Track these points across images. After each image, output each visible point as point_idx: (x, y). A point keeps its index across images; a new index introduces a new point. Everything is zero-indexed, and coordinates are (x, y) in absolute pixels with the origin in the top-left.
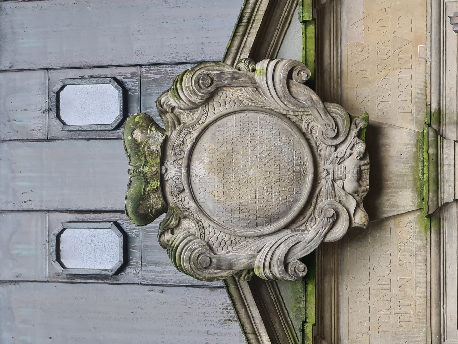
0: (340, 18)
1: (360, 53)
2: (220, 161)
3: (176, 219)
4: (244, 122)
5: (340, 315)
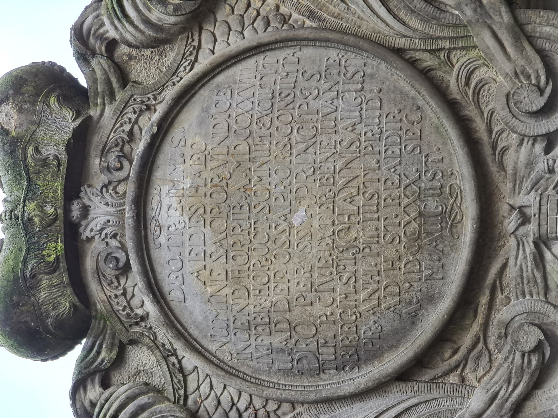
3: (110, 346)
4: (285, 74)
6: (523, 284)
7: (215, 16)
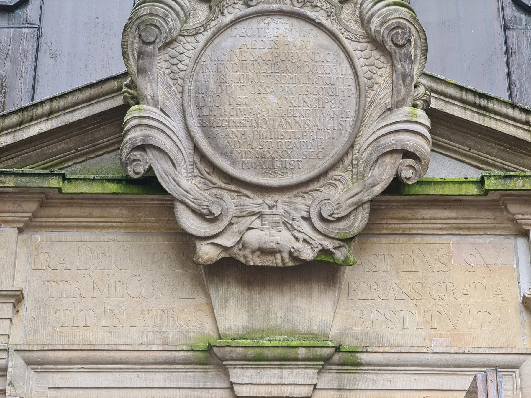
0: (487, 233)
1: (437, 260)
2: (288, 55)
4: (343, 90)
5: (75, 230)
6: (240, 206)
7: (374, 50)
